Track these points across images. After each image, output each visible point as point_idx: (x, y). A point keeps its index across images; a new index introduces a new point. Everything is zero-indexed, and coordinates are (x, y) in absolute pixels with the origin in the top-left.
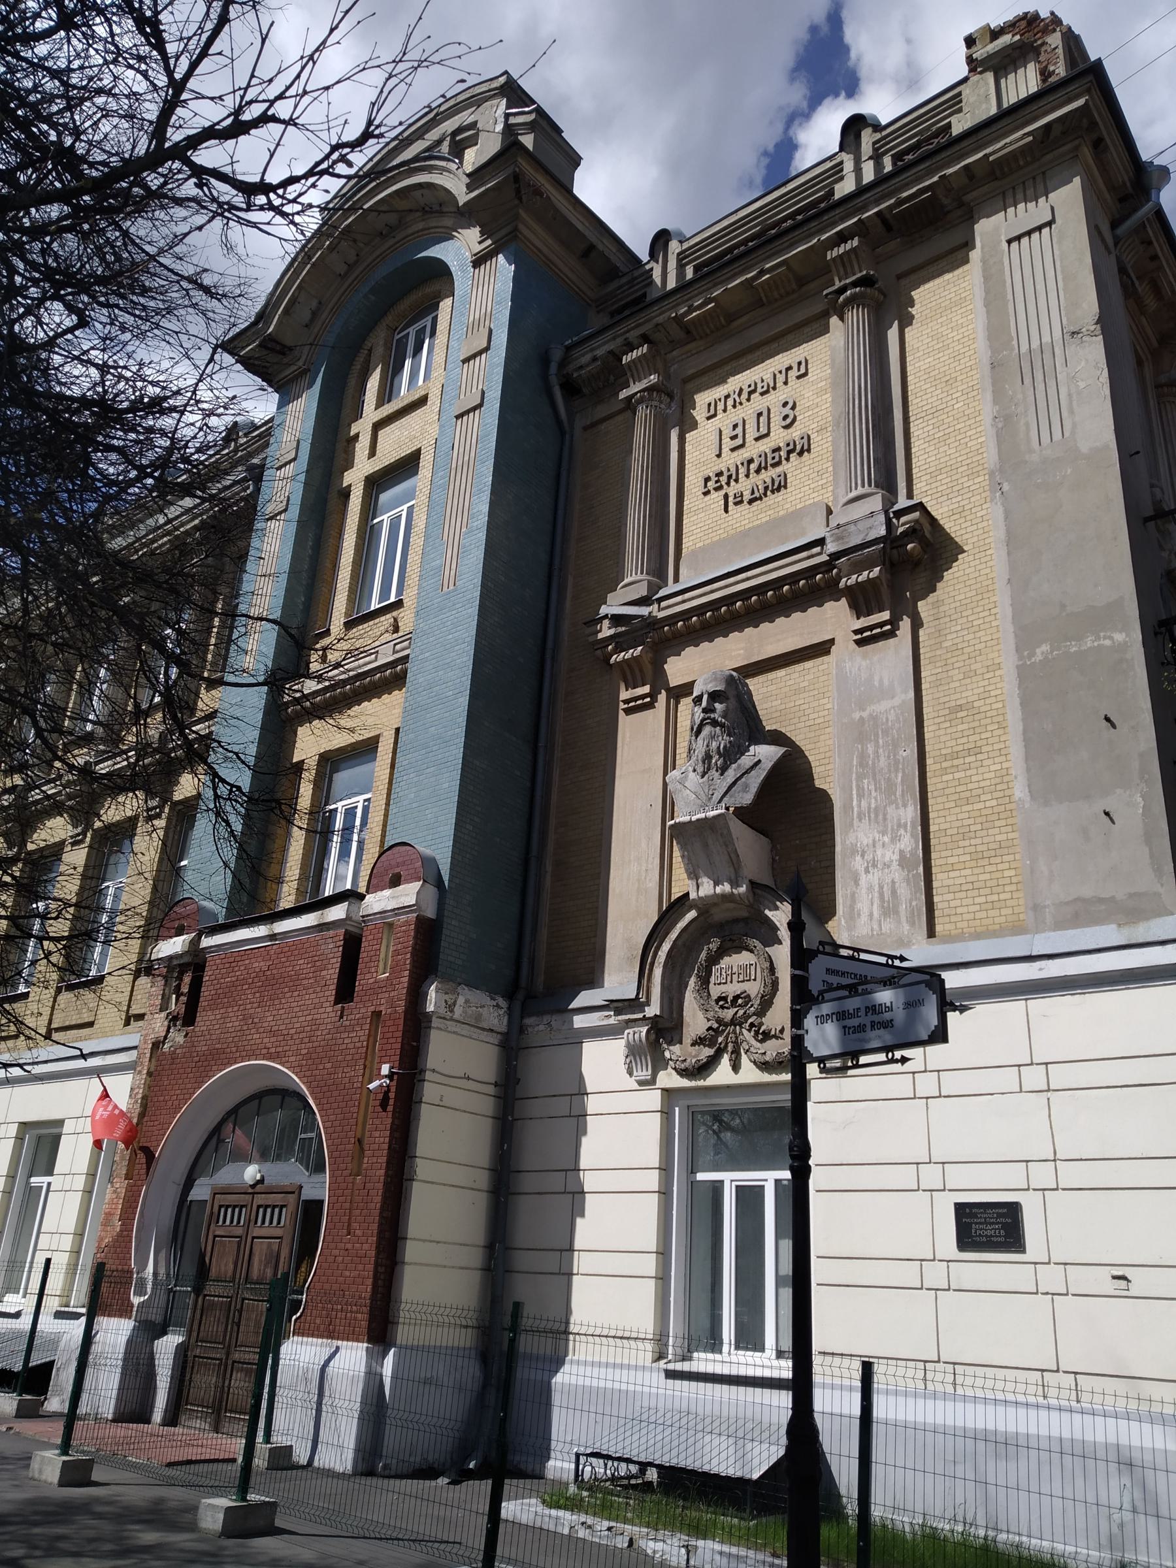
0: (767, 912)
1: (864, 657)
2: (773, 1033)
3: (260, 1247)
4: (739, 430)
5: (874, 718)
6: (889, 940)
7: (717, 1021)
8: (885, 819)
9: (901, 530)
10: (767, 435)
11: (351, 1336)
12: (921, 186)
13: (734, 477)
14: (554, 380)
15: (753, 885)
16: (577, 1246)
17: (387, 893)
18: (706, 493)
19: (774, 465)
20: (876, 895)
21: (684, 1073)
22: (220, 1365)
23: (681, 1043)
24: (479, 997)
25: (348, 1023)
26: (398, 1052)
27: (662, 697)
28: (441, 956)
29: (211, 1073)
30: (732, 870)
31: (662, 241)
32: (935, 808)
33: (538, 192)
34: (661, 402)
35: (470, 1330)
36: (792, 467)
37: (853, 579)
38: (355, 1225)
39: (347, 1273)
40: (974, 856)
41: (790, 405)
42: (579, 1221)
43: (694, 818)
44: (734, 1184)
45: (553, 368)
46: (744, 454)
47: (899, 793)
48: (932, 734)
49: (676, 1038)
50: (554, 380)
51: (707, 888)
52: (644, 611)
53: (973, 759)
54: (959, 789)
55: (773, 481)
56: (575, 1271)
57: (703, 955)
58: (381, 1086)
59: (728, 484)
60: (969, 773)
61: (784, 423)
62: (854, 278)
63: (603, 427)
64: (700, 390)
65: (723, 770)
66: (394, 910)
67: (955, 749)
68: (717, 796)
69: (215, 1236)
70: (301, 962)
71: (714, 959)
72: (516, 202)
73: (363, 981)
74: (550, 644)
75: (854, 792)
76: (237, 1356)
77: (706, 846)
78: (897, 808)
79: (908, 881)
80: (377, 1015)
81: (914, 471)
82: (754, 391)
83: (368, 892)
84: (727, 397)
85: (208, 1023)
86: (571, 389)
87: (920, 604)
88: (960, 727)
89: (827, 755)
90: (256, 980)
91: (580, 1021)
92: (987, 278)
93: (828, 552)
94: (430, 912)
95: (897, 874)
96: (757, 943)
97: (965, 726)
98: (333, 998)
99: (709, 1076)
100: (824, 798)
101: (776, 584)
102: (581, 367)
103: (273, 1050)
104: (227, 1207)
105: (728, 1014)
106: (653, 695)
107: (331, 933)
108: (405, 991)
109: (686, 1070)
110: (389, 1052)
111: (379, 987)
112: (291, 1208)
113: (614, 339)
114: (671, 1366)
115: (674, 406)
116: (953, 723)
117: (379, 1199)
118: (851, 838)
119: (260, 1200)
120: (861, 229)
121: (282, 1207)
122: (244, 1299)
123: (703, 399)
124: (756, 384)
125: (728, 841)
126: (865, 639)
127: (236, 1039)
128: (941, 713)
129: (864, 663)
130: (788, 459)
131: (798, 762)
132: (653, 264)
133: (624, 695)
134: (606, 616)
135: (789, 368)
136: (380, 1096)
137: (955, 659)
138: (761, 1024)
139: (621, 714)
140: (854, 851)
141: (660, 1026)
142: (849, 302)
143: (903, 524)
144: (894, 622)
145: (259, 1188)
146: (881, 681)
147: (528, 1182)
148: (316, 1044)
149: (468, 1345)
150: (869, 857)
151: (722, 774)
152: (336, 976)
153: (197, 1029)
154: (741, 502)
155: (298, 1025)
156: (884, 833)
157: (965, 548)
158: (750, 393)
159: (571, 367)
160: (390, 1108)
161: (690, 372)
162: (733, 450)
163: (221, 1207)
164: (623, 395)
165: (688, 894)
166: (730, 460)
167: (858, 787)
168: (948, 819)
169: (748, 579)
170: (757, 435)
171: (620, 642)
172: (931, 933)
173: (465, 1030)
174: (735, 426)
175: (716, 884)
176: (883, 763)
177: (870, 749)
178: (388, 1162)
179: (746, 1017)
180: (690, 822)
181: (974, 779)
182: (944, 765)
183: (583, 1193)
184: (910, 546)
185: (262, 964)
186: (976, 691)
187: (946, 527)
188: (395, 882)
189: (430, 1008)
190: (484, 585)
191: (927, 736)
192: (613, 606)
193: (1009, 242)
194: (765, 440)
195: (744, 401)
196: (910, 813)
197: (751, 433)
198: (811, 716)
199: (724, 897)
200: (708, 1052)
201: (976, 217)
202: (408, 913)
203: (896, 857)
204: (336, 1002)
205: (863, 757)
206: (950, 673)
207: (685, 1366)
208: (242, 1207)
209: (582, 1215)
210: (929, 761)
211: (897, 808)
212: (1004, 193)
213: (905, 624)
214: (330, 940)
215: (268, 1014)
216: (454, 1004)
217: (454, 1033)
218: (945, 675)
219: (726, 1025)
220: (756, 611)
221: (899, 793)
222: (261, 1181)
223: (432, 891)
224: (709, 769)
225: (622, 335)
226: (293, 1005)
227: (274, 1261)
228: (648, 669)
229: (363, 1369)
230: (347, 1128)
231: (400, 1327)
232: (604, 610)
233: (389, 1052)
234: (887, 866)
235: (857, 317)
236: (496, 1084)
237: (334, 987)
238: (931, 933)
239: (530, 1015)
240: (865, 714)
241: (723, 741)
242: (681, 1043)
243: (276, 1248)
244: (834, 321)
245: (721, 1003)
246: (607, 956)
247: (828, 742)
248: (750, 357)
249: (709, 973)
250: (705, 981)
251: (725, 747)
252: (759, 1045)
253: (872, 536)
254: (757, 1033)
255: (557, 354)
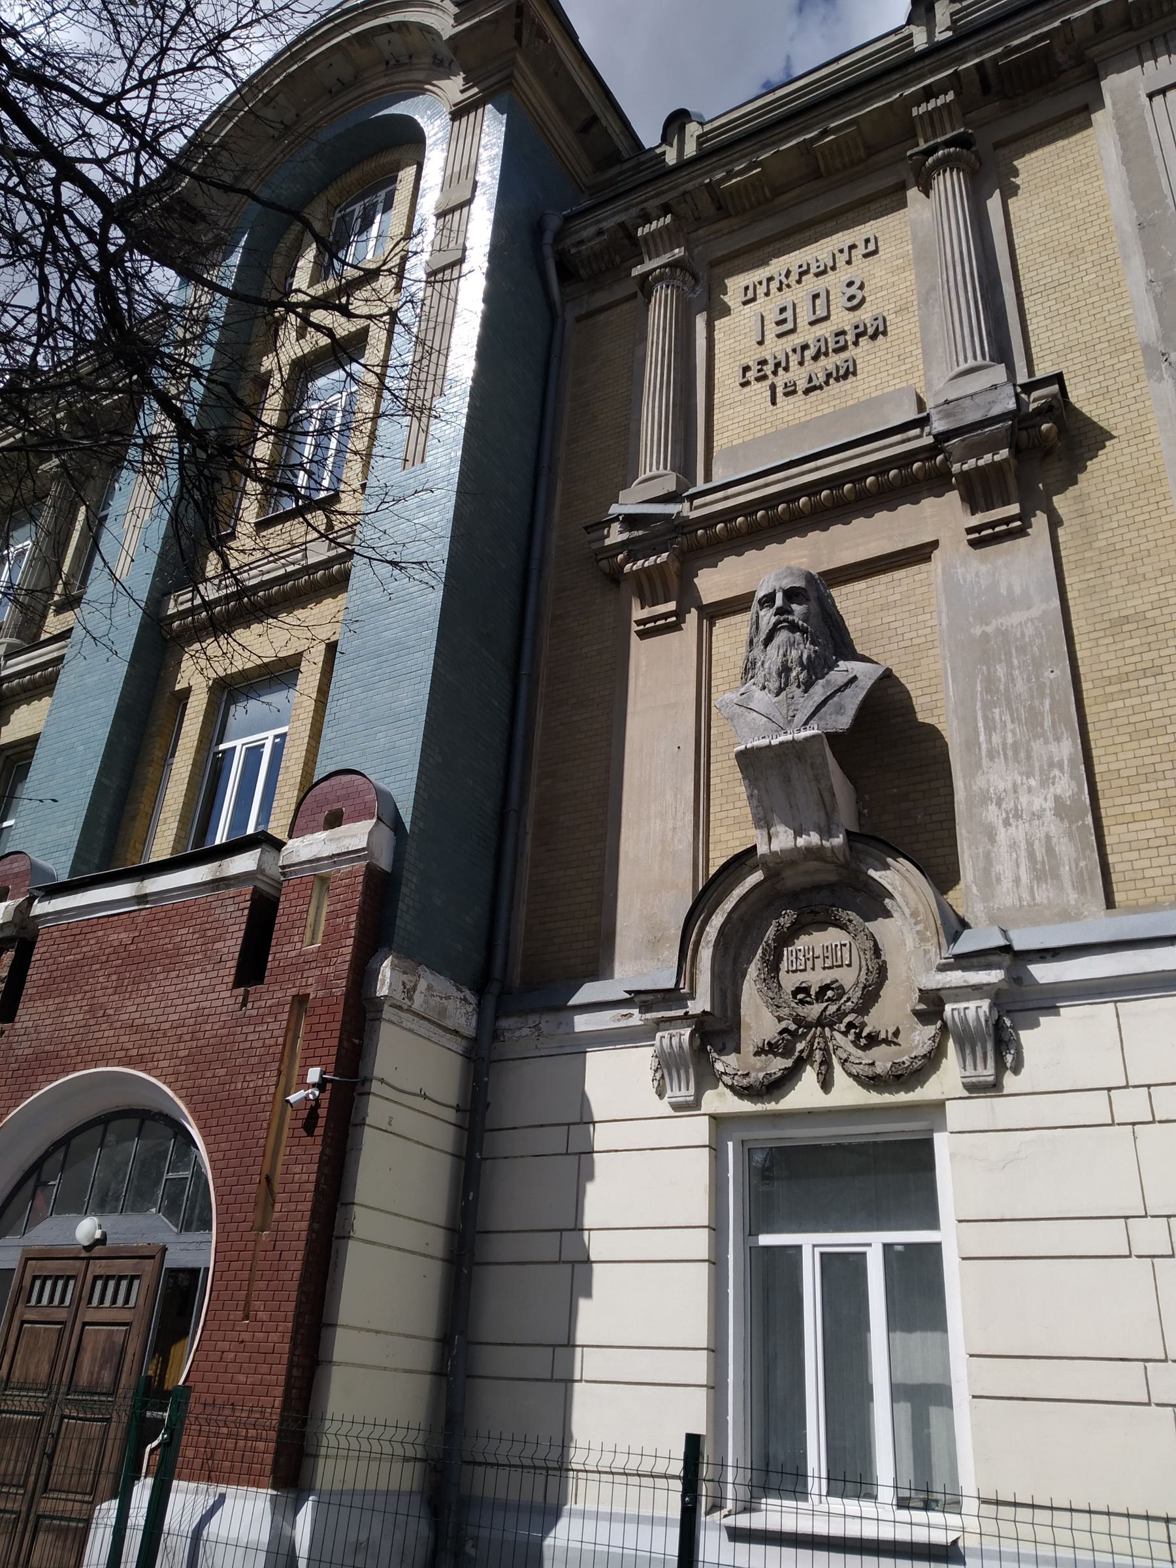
0: (871, 872)
1: (983, 561)
2: (882, 1036)
3: (95, 1339)
4: (789, 314)
5: (1003, 633)
6: (1047, 912)
7: (794, 1021)
8: (1029, 757)
9: (1032, 406)
10: (826, 318)
11: (247, 1477)
12: (1037, 32)
13: (783, 364)
14: (548, 251)
15: (849, 834)
16: (581, 1337)
17: (322, 835)
18: (744, 385)
19: (836, 351)
20: (1023, 854)
21: (743, 1092)
22: (16, 1520)
23: (738, 1050)
24: (443, 985)
25: (254, 1012)
26: (334, 1051)
27: (692, 617)
28: (398, 922)
29: (36, 1086)
30: (822, 814)
31: (676, 125)
32: (1100, 743)
33: (541, 34)
34: (684, 282)
35: (409, 1466)
36: (863, 353)
37: (971, 463)
38: (257, 1305)
39: (242, 1378)
40: (1164, 803)
41: (857, 284)
42: (583, 1304)
43: (775, 742)
44: (818, 1250)
45: (548, 238)
46: (796, 340)
47: (1047, 723)
48: (1087, 653)
49: (730, 1045)
50: (548, 251)
51: (783, 839)
52: (672, 509)
53: (1151, 681)
54: (1133, 719)
55: (837, 368)
56: (577, 1376)
57: (771, 932)
58: (306, 1098)
59: (775, 373)
60: (1146, 699)
61: (849, 305)
62: (948, 136)
63: (602, 317)
64: (732, 273)
65: (808, 686)
66: (334, 856)
67: (1124, 670)
68: (801, 717)
69: (23, 1322)
70: (185, 931)
71: (786, 938)
72: (515, 43)
73: (281, 953)
74: (536, 554)
75: (981, 724)
76: (45, 1505)
77: (787, 780)
78: (1046, 742)
79: (1071, 837)
80: (301, 1001)
81: (1033, 351)
82: (807, 272)
83: (290, 837)
84: (770, 279)
85: (36, 1017)
86: (566, 273)
87: (1055, 498)
88: (1128, 643)
89: (934, 681)
90: (112, 957)
91: (583, 1023)
92: (1123, 136)
93: (934, 432)
94: (384, 862)
95: (1053, 827)
96: (853, 915)
97: (1137, 641)
98: (232, 978)
99: (783, 1097)
100: (932, 735)
101: (857, 474)
102: (582, 242)
103: (135, 1052)
104: (45, 1279)
105: (813, 1011)
106: (680, 614)
107: (232, 891)
108: (346, 966)
109: (749, 1088)
110: (319, 1052)
111: (302, 964)
112: (147, 1280)
113: (626, 209)
114: (730, 1521)
115: (699, 290)
116: (1117, 638)
117: (298, 1265)
118: (980, 782)
119: (97, 1268)
120: (955, 81)
121: (133, 1278)
122: (63, 1417)
123: (735, 285)
124: (808, 265)
125: (820, 776)
126: (981, 539)
127: (78, 1038)
128: (1098, 627)
129: (983, 569)
130: (856, 343)
131: (890, 691)
132: (665, 148)
133: (638, 613)
134: (616, 519)
135: (852, 247)
136: (304, 1114)
137: (1112, 562)
138: (864, 1025)
139: (634, 638)
140: (985, 798)
141: (707, 1028)
142: (941, 165)
143: (1035, 400)
144: (1025, 517)
145: (98, 1251)
146: (1010, 588)
147: (501, 1248)
148: (201, 1043)
149: (406, 1487)
150: (1008, 805)
151: (806, 691)
152: (238, 948)
153: (18, 1025)
154: (794, 392)
155: (176, 1017)
156: (1029, 775)
157: (1115, 433)
158: (801, 274)
159: (569, 241)
160: (319, 1131)
161: (720, 254)
162: (779, 336)
163: (35, 1278)
164: (637, 271)
165: (755, 847)
166: (775, 348)
167: (986, 719)
168: (1121, 756)
169: (817, 469)
170: (813, 318)
171: (633, 549)
172: (1110, 903)
173: (424, 1028)
174: (783, 310)
175: (798, 833)
176: (1020, 687)
177: (1001, 671)
178: (314, 1211)
179: (840, 1015)
180: (769, 746)
181: (1154, 706)
182: (1109, 689)
183: (588, 1262)
184: (1044, 427)
185: (123, 935)
186: (1146, 599)
187: (1084, 411)
188: (334, 820)
189: (382, 990)
190: (464, 461)
191: (1079, 655)
192: (629, 503)
193: (1151, 96)
194: (823, 325)
195: (793, 283)
196: (1067, 748)
197: (805, 316)
198: (907, 636)
199: (811, 853)
200: (778, 1065)
201: (1102, 73)
202: (352, 860)
203: (1050, 804)
204: (237, 984)
205: (990, 684)
206: (1108, 579)
207: (756, 1521)
208: (69, 1278)
209: (588, 1294)
210: (1085, 686)
211: (1046, 742)
212: (1138, 47)
213: (1040, 521)
214: (230, 901)
215: (127, 1003)
216: (414, 989)
217: (410, 1030)
218: (1100, 581)
219: (809, 1026)
220: (828, 509)
221: (1047, 723)
222: (102, 1241)
223: (386, 833)
224: (786, 685)
225: (637, 204)
226: (167, 989)
227: (115, 1359)
228: (674, 582)
229: (265, 1538)
230: (249, 1161)
231: (321, 1461)
232: (615, 509)
233: (319, 1052)
234: (1038, 816)
235: (948, 184)
236: (458, 1109)
237: (234, 963)
238: (1110, 903)
239: (508, 1015)
240: (989, 629)
241: (806, 650)
242: (738, 1050)
243: (119, 1339)
244: (913, 193)
245: (800, 996)
246: (618, 939)
247: (933, 667)
248: (798, 237)
249: (779, 958)
250: (773, 967)
251: (809, 657)
252: (860, 1053)
253: (996, 410)
254: (858, 1036)
255: (553, 222)
